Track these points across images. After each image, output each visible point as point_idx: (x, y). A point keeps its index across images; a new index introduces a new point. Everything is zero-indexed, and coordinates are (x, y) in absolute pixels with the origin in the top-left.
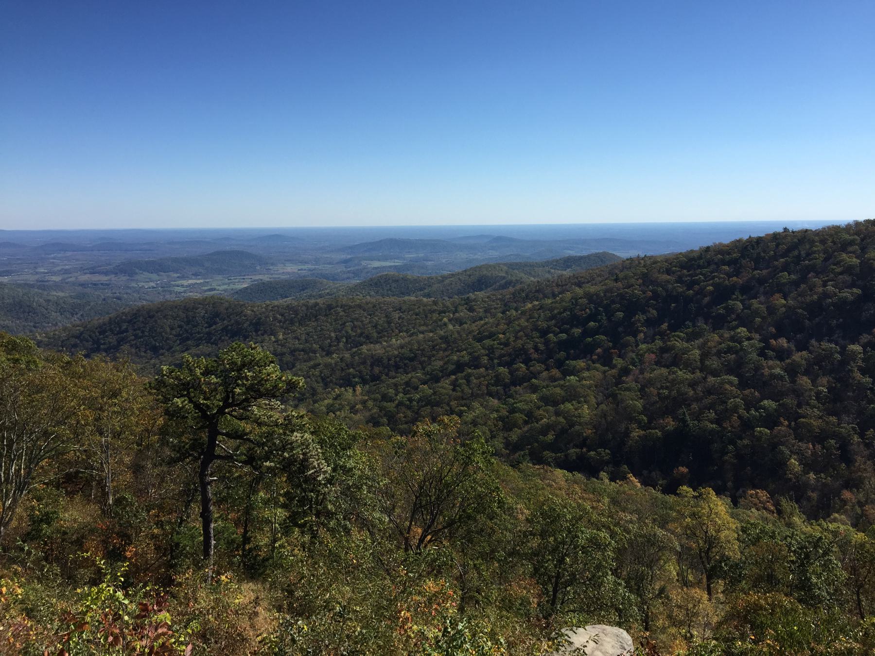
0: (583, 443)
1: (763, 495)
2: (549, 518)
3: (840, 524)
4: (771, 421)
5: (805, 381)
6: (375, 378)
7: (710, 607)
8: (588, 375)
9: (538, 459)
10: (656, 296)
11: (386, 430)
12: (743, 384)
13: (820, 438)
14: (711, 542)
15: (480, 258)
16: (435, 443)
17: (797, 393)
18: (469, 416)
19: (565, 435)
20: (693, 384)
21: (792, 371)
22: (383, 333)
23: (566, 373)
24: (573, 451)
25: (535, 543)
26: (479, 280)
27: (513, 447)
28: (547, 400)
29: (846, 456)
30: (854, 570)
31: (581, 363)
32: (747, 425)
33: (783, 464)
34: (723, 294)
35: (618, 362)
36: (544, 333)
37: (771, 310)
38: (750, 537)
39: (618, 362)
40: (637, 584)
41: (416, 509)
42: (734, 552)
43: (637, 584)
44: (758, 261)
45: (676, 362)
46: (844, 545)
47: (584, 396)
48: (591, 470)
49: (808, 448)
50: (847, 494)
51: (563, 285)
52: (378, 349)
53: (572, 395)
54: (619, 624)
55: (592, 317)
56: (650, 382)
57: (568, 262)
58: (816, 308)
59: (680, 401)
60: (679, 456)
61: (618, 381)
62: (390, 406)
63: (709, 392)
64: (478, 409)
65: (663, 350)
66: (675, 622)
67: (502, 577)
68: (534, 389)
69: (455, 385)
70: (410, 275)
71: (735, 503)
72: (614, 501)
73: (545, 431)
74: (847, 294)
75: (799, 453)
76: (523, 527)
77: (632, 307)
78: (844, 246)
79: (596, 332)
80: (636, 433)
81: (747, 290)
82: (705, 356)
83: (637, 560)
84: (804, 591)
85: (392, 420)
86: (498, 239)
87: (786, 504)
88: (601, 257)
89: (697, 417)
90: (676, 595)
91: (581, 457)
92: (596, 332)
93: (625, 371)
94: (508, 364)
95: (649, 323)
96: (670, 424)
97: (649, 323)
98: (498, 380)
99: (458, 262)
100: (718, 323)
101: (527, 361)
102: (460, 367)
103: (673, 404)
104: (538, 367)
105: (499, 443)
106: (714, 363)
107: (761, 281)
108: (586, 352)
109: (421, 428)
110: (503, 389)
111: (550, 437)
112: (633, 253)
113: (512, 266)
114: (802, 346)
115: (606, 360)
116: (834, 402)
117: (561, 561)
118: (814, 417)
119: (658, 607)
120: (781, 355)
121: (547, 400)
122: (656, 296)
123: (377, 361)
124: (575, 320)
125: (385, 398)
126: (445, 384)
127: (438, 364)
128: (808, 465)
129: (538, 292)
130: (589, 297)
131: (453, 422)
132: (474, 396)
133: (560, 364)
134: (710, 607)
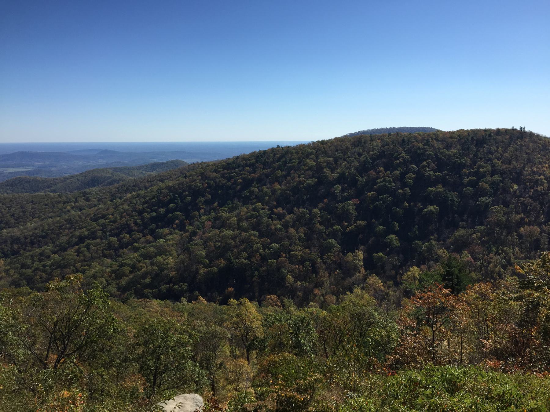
0: (170, 281)
1: (274, 297)
2: (148, 333)
3: (314, 308)
4: (276, 255)
5: (292, 230)
6: (15, 253)
7: (249, 368)
8: (171, 238)
9: (140, 295)
10: (209, 186)
11: (25, 289)
12: (261, 236)
13: (302, 262)
14: (248, 329)
15: (92, 164)
16: (65, 295)
17: (289, 238)
18: (91, 272)
19: (158, 277)
20: (234, 238)
21: (286, 226)
22: (19, 220)
23: (157, 237)
24: (164, 287)
25: (140, 351)
26: (92, 179)
27: (123, 289)
28: (145, 256)
29: (315, 270)
30: (322, 332)
31: (166, 231)
32: (264, 259)
33: (283, 279)
34: (247, 184)
35: (189, 228)
36: (140, 213)
37: (274, 192)
38: (268, 323)
39: (189, 228)
40: (206, 363)
41: (53, 340)
42: (260, 333)
43: (206, 363)
44: (265, 165)
45: (223, 226)
46: (316, 319)
47: (169, 250)
48: (175, 297)
49: (296, 267)
50: (316, 291)
51: (151, 181)
52: (16, 232)
53: (161, 251)
54: (196, 391)
55: (171, 201)
56: (209, 239)
57: (154, 166)
58: (296, 190)
59: (227, 248)
60: (227, 281)
61: (190, 240)
62: (29, 272)
63: (243, 242)
64: (96, 267)
65: (216, 219)
66: (229, 381)
67: (119, 377)
68: (136, 250)
69: (78, 252)
70: (39, 177)
71: (260, 304)
72: (191, 315)
73: (144, 276)
74: (310, 182)
75: (292, 271)
76: (132, 341)
77: (196, 193)
78: (308, 156)
79: (174, 210)
80: (202, 271)
81: (260, 181)
82: (239, 220)
83: (205, 349)
84: (298, 349)
85: (30, 281)
86: (105, 151)
87: (286, 301)
88: (175, 163)
89: (237, 257)
90: (229, 365)
91: (169, 290)
92: (174, 210)
93: (194, 233)
94: (117, 235)
95: (207, 203)
96: (222, 262)
97: (207, 203)
98: (110, 246)
99: (76, 167)
100: (246, 201)
101: (130, 232)
102: (81, 239)
103: (222, 251)
104: (138, 235)
105: (113, 288)
106: (245, 224)
107: (267, 176)
108: (169, 223)
109: (52, 285)
110: (114, 251)
111: (148, 280)
112: (194, 161)
113: (115, 170)
114: (290, 212)
115: (182, 228)
116: (307, 242)
117: (158, 358)
118: (298, 251)
119: (220, 375)
120: (280, 217)
121: (145, 256)
122: (209, 186)
123: (15, 240)
124: (161, 204)
125: (24, 266)
126: (71, 253)
127: (64, 239)
128: (297, 278)
129: (134, 186)
130: (169, 188)
131: (77, 279)
132: (93, 258)
133: (152, 232)
134: (249, 368)
